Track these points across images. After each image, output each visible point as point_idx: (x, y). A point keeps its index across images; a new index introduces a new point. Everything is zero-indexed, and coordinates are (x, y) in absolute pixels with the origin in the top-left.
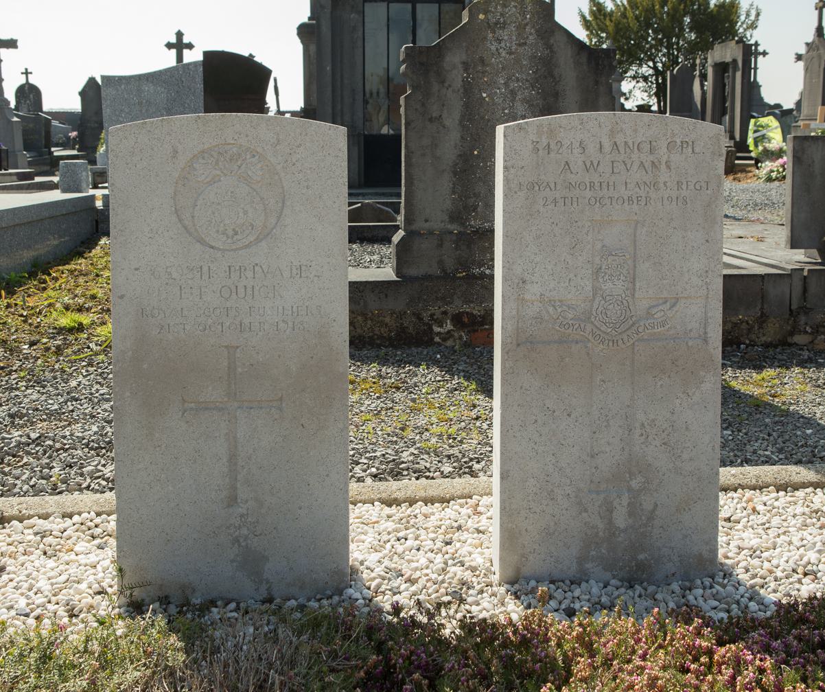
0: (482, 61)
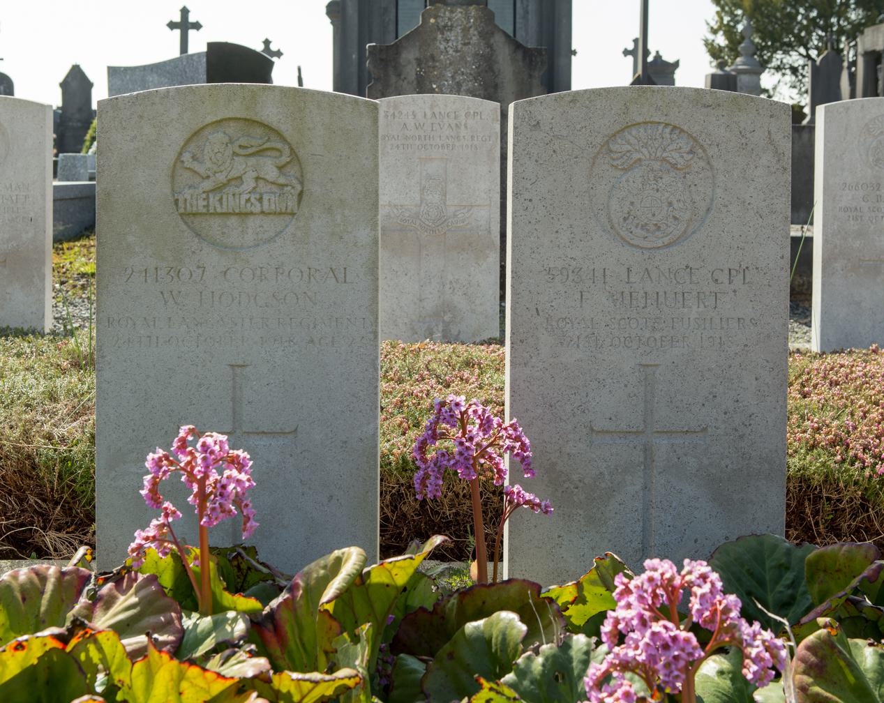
0: (433, 58)
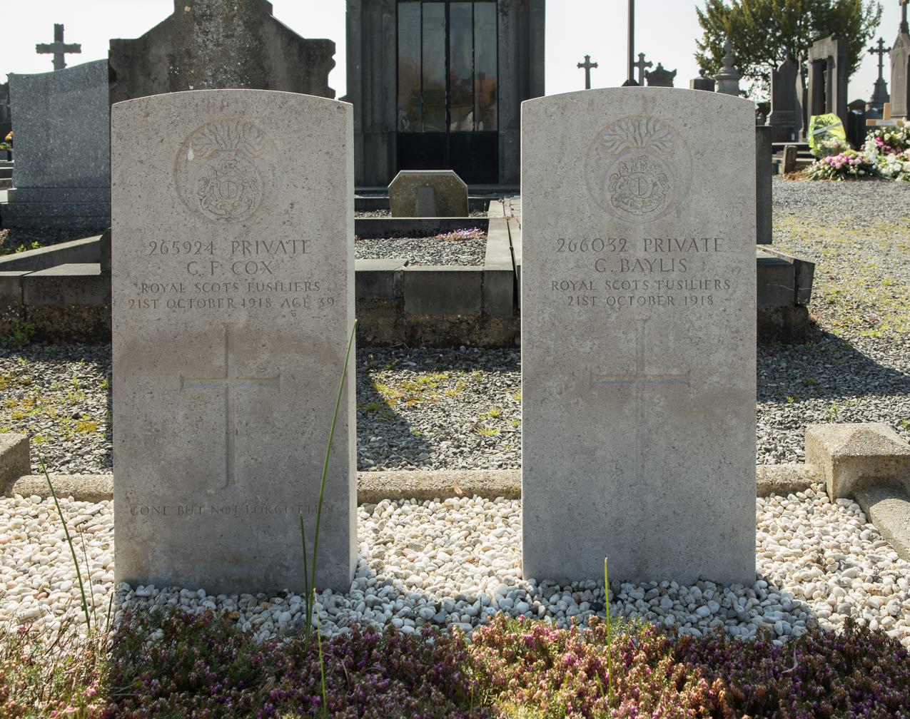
0: (188, 53)
